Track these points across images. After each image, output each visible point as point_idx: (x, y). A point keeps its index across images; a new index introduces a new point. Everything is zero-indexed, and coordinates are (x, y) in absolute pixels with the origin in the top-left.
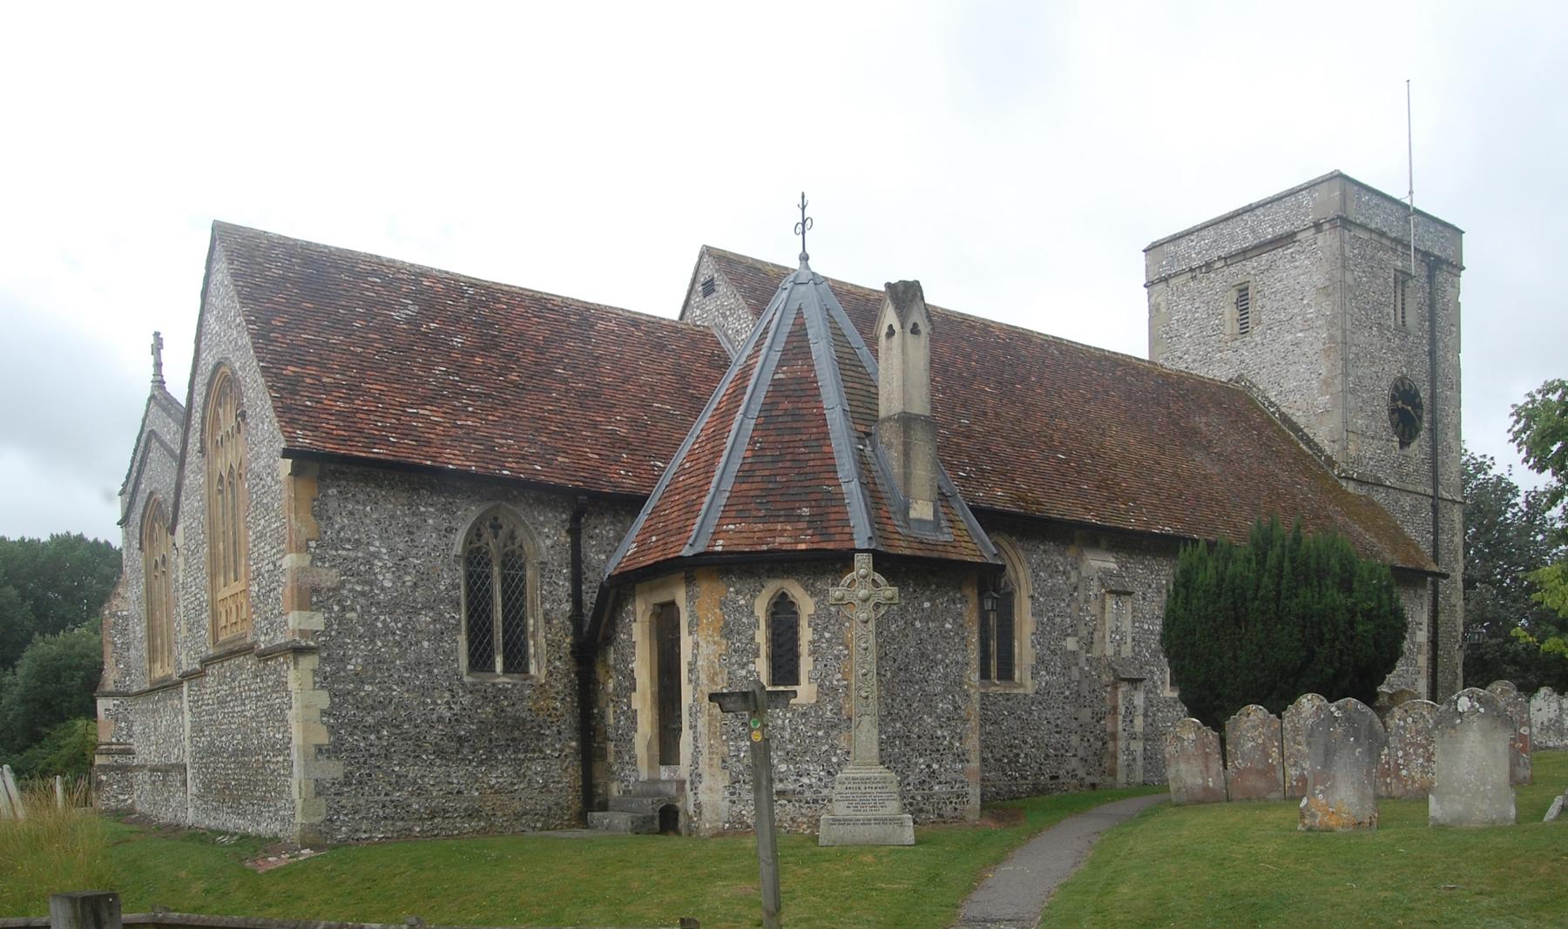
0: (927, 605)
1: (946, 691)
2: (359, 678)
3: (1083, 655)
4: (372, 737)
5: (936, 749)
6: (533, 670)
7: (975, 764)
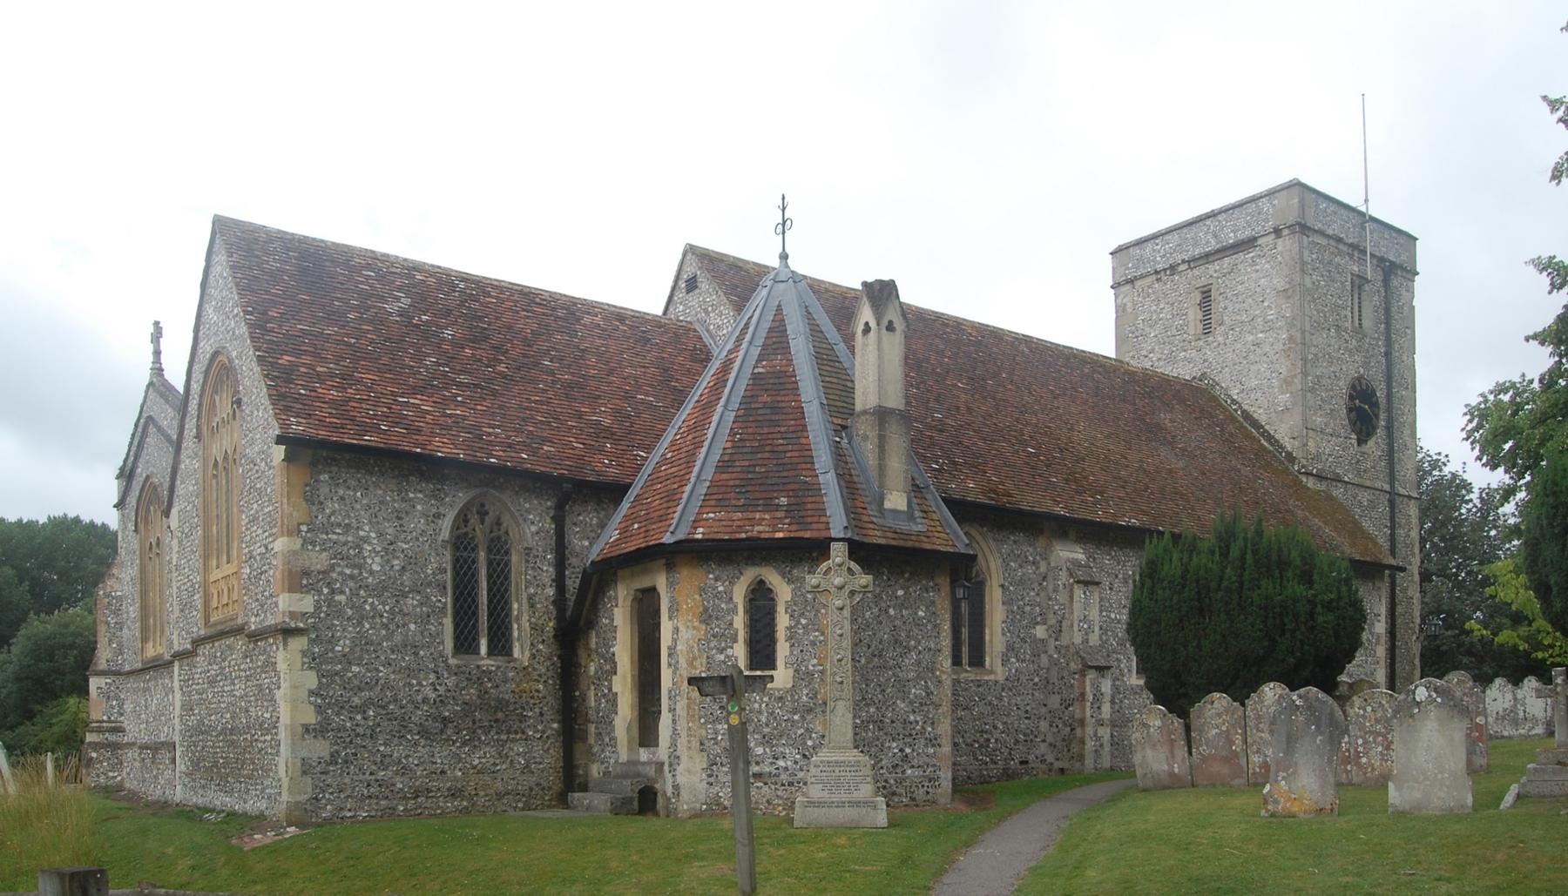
0: (900, 593)
1: (919, 677)
2: (347, 660)
3: (1052, 644)
4: (359, 717)
6: (516, 653)
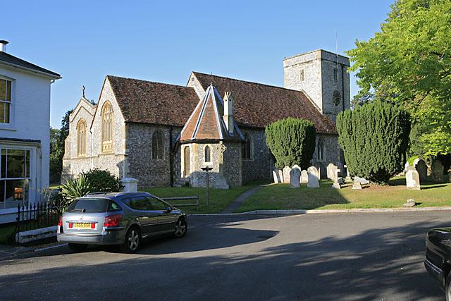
2: (135, 161)
5: (233, 173)
7: (241, 176)
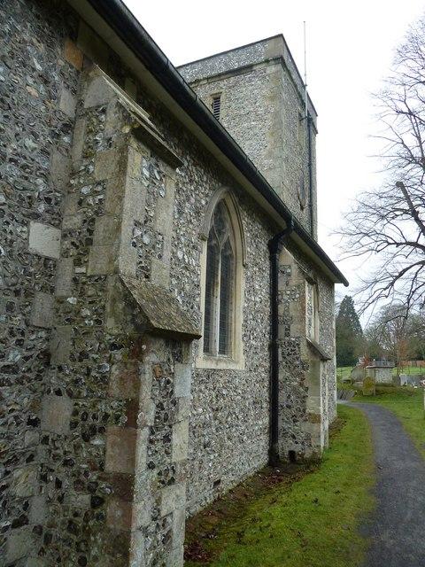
3: (67, 271)
